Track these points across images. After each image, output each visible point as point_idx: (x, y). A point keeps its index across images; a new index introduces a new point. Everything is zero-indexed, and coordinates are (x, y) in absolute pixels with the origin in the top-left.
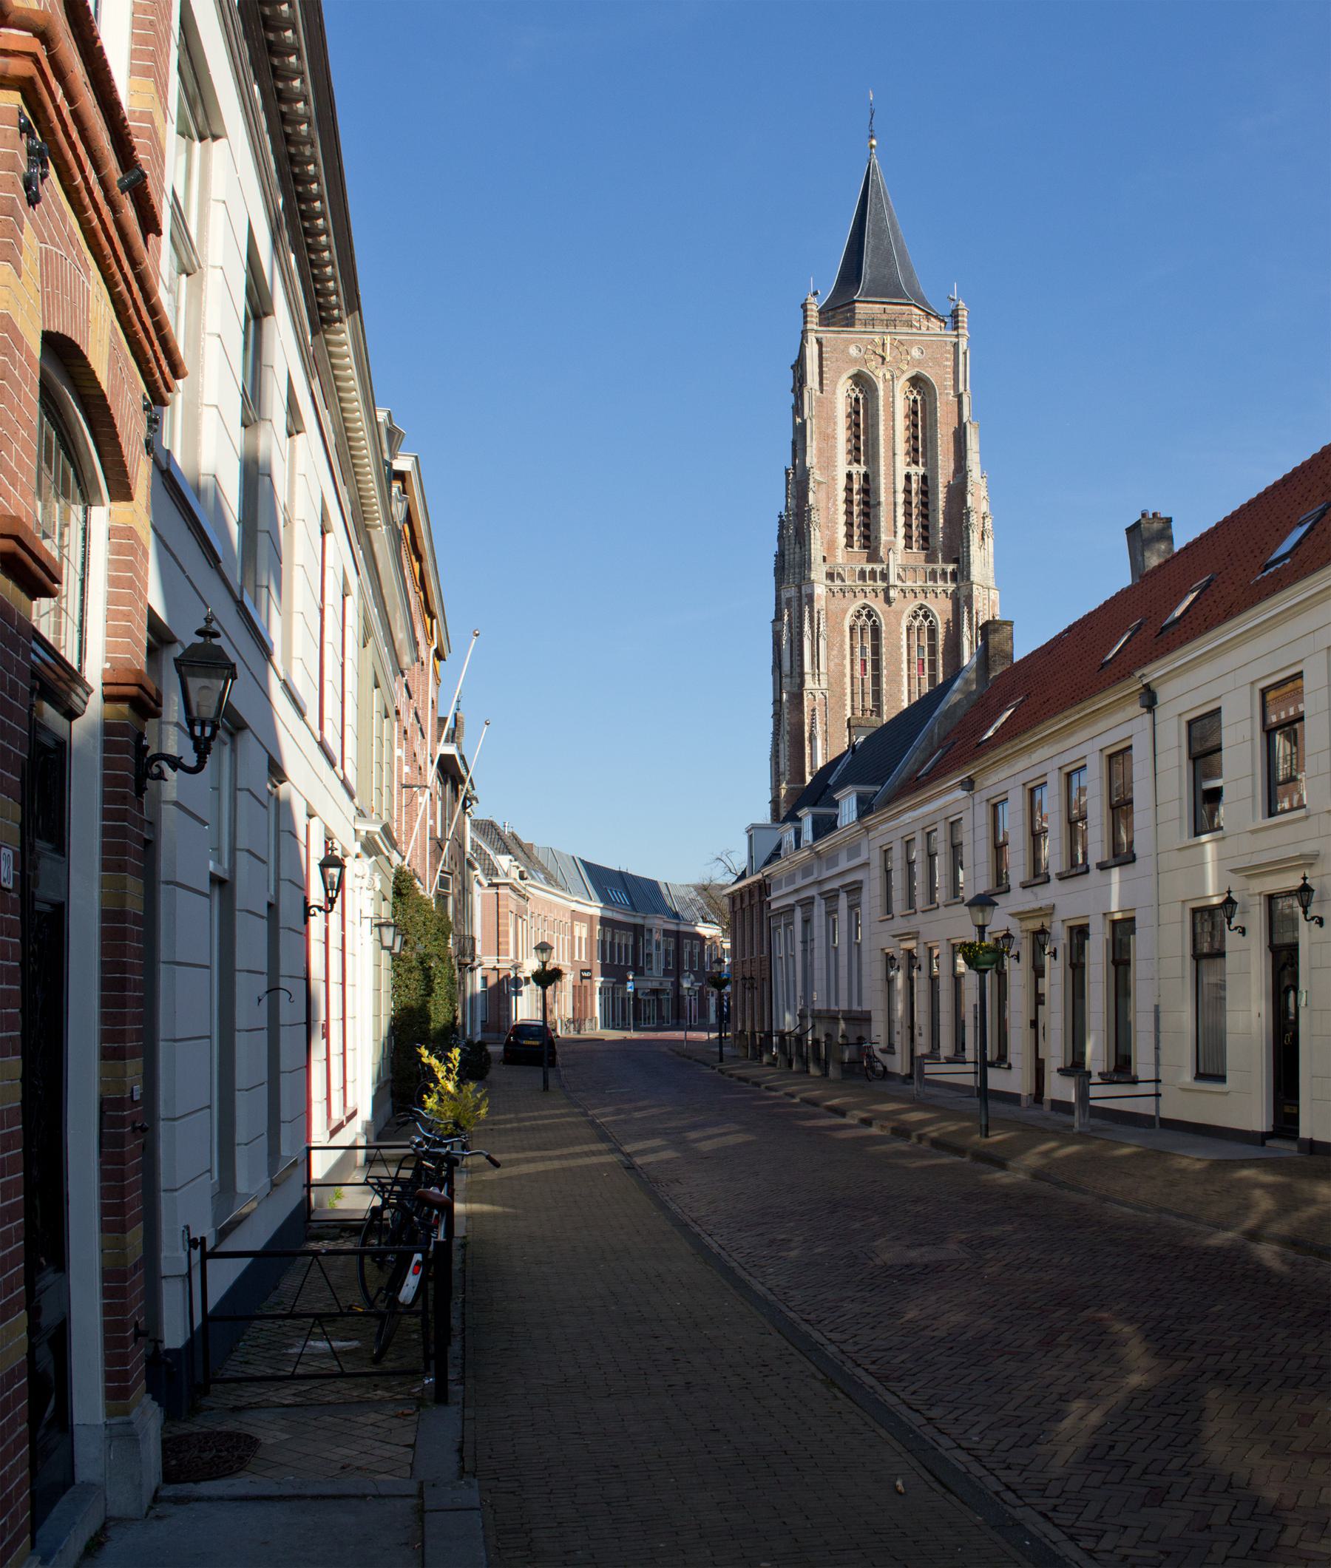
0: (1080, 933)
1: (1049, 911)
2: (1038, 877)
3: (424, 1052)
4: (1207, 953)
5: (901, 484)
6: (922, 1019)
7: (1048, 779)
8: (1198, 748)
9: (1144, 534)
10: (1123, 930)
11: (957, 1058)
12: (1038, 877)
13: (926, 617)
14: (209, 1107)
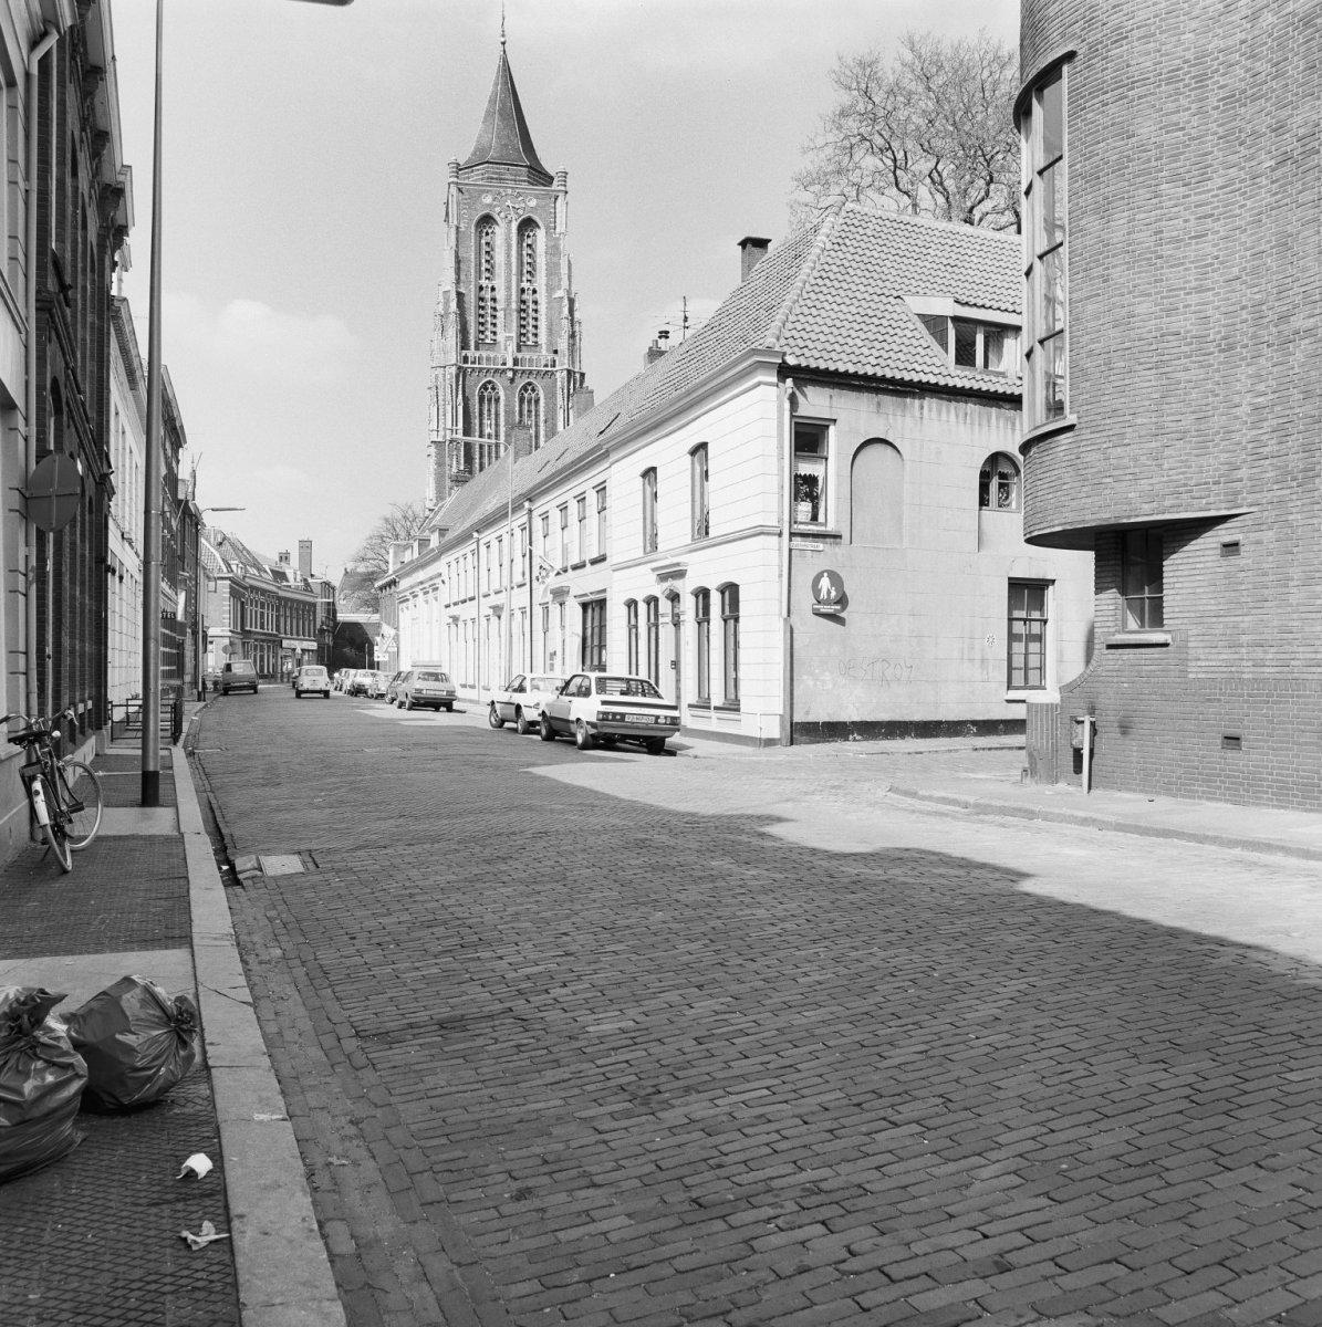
13: (533, 390)
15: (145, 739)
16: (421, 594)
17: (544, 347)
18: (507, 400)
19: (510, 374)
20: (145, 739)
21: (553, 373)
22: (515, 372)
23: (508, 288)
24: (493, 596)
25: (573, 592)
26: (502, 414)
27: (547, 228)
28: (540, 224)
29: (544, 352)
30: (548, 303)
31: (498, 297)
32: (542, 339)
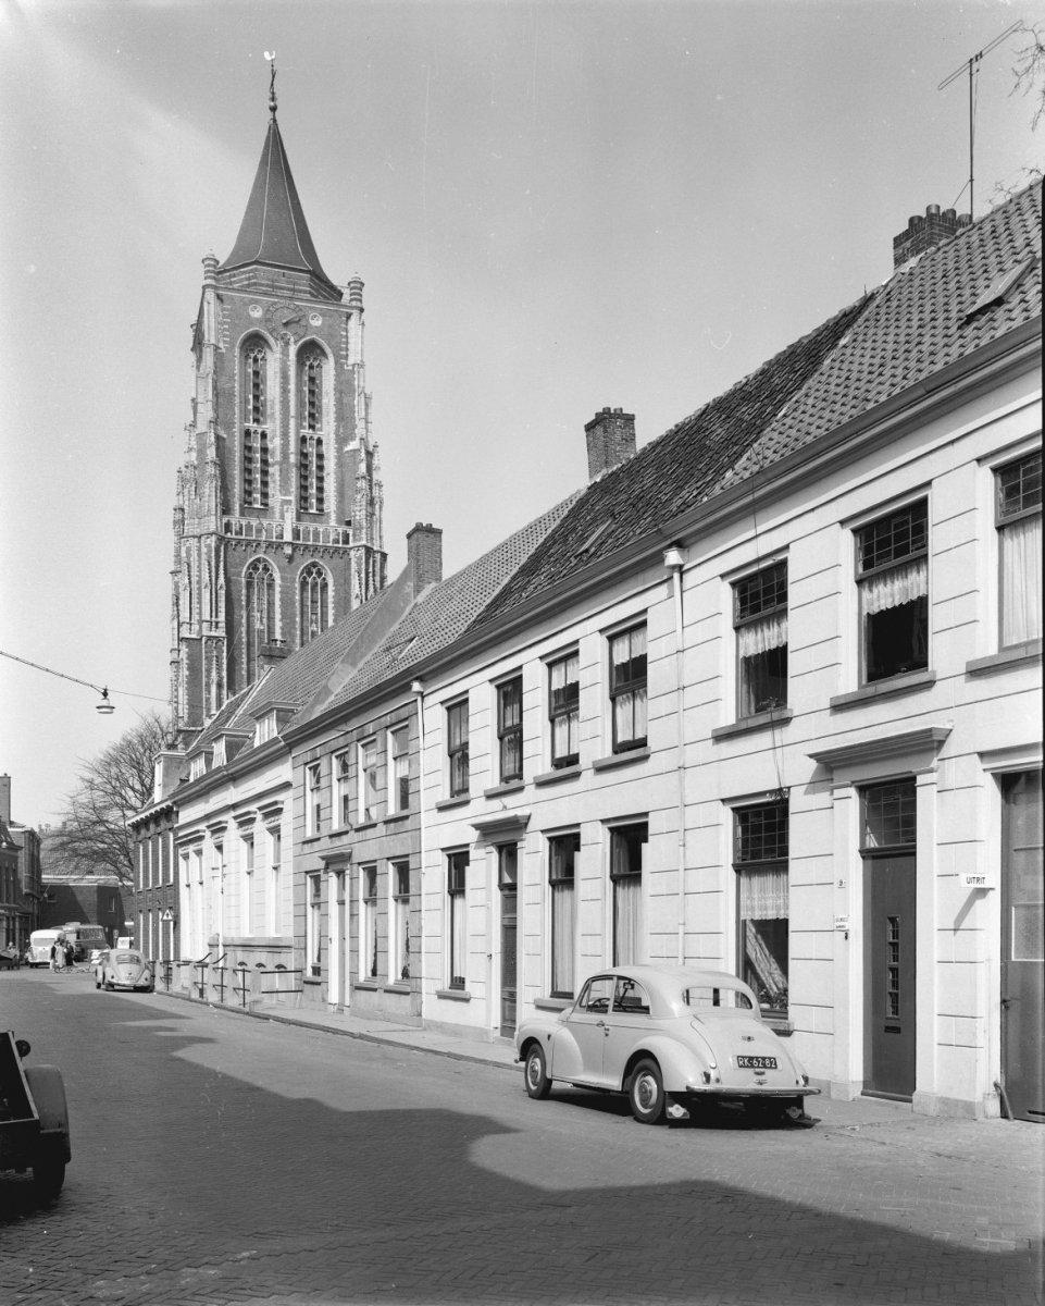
9: (607, 425)
16: (232, 825)
17: (333, 517)
19: (288, 550)
22: (295, 547)
23: (285, 435)
26: (278, 603)
28: (328, 350)
32: (331, 504)
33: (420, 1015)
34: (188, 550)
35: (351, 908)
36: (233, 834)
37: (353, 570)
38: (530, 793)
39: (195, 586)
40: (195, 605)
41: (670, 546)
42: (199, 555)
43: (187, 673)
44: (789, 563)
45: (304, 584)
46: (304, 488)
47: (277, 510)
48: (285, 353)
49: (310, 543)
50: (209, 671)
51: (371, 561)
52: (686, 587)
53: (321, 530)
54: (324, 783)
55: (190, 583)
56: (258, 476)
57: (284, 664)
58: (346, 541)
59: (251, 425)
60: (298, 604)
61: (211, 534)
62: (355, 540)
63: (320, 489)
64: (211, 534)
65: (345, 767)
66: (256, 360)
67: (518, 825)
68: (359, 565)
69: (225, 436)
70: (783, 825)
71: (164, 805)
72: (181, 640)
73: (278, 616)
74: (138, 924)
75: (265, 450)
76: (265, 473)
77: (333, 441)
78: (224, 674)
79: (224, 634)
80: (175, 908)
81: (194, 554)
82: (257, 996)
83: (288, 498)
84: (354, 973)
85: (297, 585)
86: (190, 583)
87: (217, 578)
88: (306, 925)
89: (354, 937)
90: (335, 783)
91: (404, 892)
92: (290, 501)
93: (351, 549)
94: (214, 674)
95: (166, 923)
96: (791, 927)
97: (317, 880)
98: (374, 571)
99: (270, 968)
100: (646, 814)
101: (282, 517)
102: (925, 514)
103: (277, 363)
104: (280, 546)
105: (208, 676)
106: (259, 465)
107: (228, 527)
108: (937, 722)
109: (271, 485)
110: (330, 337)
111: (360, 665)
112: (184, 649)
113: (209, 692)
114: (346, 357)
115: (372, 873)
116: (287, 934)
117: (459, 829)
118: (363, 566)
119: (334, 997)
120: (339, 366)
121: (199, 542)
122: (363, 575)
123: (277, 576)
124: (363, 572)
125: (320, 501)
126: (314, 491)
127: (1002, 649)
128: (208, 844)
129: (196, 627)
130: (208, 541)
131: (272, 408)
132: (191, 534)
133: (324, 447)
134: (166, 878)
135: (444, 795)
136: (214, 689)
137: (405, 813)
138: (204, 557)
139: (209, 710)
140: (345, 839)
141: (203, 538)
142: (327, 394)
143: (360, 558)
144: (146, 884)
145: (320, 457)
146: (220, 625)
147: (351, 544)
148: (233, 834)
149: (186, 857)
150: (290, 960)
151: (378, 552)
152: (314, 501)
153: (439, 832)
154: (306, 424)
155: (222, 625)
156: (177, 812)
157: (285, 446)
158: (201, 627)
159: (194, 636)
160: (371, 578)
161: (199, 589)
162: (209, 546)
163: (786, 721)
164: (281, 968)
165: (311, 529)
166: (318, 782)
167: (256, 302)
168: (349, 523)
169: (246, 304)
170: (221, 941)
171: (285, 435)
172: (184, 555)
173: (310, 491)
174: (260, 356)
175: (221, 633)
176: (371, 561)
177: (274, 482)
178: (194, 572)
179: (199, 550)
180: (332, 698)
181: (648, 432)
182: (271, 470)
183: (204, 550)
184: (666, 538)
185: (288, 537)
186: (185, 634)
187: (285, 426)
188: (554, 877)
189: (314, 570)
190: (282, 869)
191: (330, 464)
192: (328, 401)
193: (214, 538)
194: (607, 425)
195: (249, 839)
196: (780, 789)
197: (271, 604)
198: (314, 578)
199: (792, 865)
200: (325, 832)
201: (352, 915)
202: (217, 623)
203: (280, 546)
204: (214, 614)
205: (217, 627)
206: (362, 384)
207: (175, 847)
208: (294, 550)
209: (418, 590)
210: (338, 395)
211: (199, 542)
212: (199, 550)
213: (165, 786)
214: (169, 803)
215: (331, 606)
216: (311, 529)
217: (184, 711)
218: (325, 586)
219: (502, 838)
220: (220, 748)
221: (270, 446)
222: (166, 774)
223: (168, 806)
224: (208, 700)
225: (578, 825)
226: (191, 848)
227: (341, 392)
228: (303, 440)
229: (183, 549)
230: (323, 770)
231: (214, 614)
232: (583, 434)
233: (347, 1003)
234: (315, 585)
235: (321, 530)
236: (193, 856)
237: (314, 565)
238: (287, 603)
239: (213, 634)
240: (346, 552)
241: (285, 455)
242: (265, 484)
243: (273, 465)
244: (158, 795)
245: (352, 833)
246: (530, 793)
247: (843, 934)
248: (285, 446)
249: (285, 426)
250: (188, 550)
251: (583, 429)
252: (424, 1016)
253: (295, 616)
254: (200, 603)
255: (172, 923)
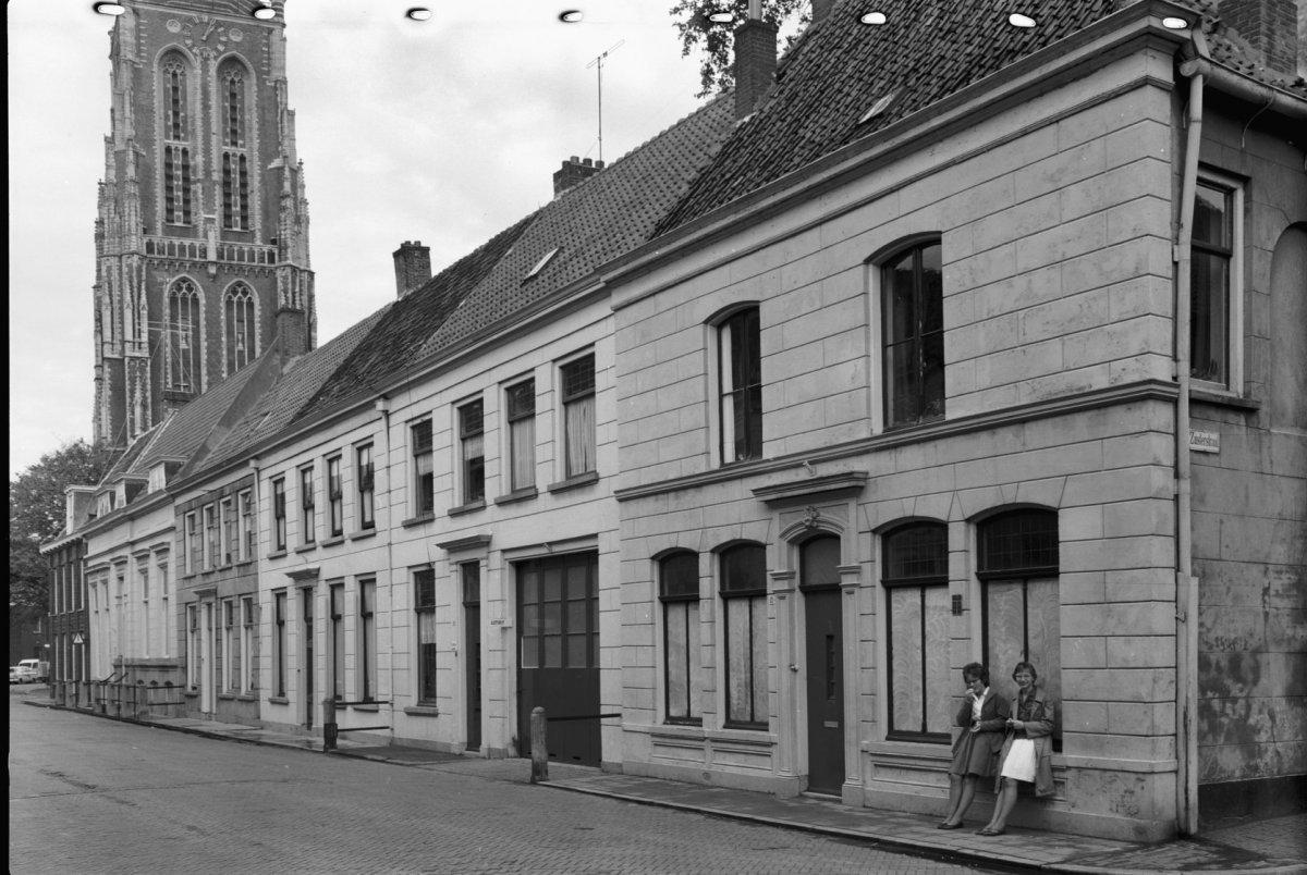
0: (336, 586)
1: (481, 542)
2: (309, 545)
3: (779, 56)
4: (425, 602)
5: (216, 164)
6: (294, 661)
7: (315, 463)
8: (512, 419)
9: (410, 257)
10: (367, 581)
11: (280, 698)
12: (309, 545)
13: (245, 293)
14: (865, 293)
15: (1243, 76)
16: (132, 560)
17: (258, 235)
18: (208, 305)
19: (213, 270)
20: (1243, 76)
21: (271, 271)
22: (220, 267)
23: (207, 152)
24: (199, 578)
25: (324, 575)
26: (203, 323)
27: (260, 74)
28: (249, 65)
29: (258, 242)
30: (262, 175)
31: (1075, 664)
32: (256, 222)
33: (259, 718)
34: (109, 269)
35: (217, 633)
36: (132, 567)
37: (279, 290)
38: (492, 512)
39: (116, 305)
40: (117, 325)
41: (378, 398)
42: (120, 274)
43: (110, 393)
44: (536, 379)
45: (229, 303)
46: (227, 206)
47: (201, 229)
48: (205, 69)
49: (235, 262)
50: (132, 392)
51: (298, 280)
52: (391, 425)
53: (246, 249)
54: (197, 530)
55: (111, 303)
56: (180, 194)
57: (190, 407)
58: (272, 260)
59: (173, 143)
60: (223, 324)
61: (133, 254)
62: (280, 260)
63: (244, 207)
64: (133, 254)
65: (212, 519)
66: (175, 75)
67: (314, 574)
68: (285, 284)
69: (144, 153)
70: (596, 562)
71: (73, 538)
72: (104, 359)
73: (203, 336)
74: (53, 647)
75: (186, 167)
76: (186, 190)
77: (256, 159)
78: (149, 394)
79: (147, 355)
80: (85, 632)
81: (115, 273)
82: (145, 708)
83: (211, 216)
84: (219, 687)
85: (223, 305)
86: (111, 303)
87: (139, 297)
88: (186, 648)
89: (219, 658)
90: (206, 532)
91: (251, 623)
92: (214, 219)
93: (276, 268)
94: (138, 395)
95: (79, 645)
96: (438, 649)
97: (193, 608)
98: (301, 290)
99: (161, 684)
100: (374, 573)
101: (206, 236)
102: (593, 364)
103: (200, 79)
104: (205, 265)
105: (132, 397)
106: (180, 183)
107: (150, 247)
108: (487, 531)
109: (193, 204)
110: (251, 53)
111: (235, 427)
112: (107, 369)
113: (133, 413)
114: (268, 73)
115: (229, 604)
116: (169, 653)
117: (422, 547)
118: (290, 286)
119: (205, 707)
120: (261, 83)
121: (120, 261)
122: (290, 295)
123: (201, 296)
124: (290, 292)
125: (244, 218)
126: (238, 209)
127: (513, 491)
128: (113, 574)
129: (118, 347)
130: (129, 261)
131: (193, 124)
132: (112, 253)
133: (248, 164)
134: (78, 605)
135: (410, 512)
136: (138, 410)
137: (230, 565)
138: (125, 276)
139: (133, 431)
140: (213, 578)
141: (124, 258)
142: (250, 110)
143: (285, 278)
144: (61, 609)
145: (243, 174)
146: (143, 345)
147: (277, 264)
148: (132, 567)
149: (94, 585)
150: (174, 677)
151: (305, 271)
152: (238, 218)
153: (272, 576)
154: (228, 140)
155: (145, 346)
156: (87, 545)
157: (208, 163)
158: (123, 347)
159: (116, 356)
160: (297, 298)
161: (121, 308)
162: (130, 266)
163: (432, 520)
164: (169, 685)
165: (236, 249)
166: (194, 529)
167: (174, 16)
168: (274, 242)
169: (164, 17)
170: (124, 663)
171: (207, 152)
172: (104, 274)
173: (233, 209)
174: (178, 72)
175: (145, 353)
176: (298, 280)
177: (197, 200)
178: (116, 292)
179: (120, 269)
180: (210, 456)
181: (439, 264)
182: (193, 187)
183: (125, 269)
184: (377, 392)
185: (212, 256)
186: (108, 354)
187: (207, 141)
188: (666, 594)
189: (240, 290)
190: (150, 602)
191: (255, 182)
192: (252, 118)
193: (136, 258)
194: (410, 257)
195: (144, 572)
196: (429, 564)
197: (196, 323)
198: (240, 298)
199: (437, 610)
200: (235, 563)
201: (217, 640)
202: (140, 343)
203: (205, 265)
204: (137, 334)
205: (140, 348)
206: (284, 100)
207: (86, 575)
208: (218, 269)
209: (284, 363)
210: (260, 111)
211: (120, 261)
212: (120, 269)
213: (76, 518)
214: (79, 535)
215: (257, 325)
216: (236, 249)
217: (107, 430)
218: (251, 305)
219: (305, 584)
220: (121, 491)
221: (192, 163)
222: (77, 507)
223: (78, 539)
224: (132, 421)
225: (343, 577)
226: (99, 578)
227: (263, 109)
228: (226, 156)
229: (104, 268)
230: (198, 520)
231: (137, 334)
232: (391, 260)
233: (214, 712)
234: (240, 304)
235: (246, 249)
236: (99, 585)
237: (239, 284)
238: (213, 323)
239: (137, 354)
240: (272, 272)
241: (208, 173)
242: (187, 201)
243: (195, 182)
244: (69, 528)
245: (217, 574)
246: (492, 512)
247: (453, 654)
248: (208, 163)
249: (207, 141)
250: (109, 269)
251: (391, 256)
252: (262, 718)
253: (221, 335)
254: (122, 322)
255: (83, 647)
